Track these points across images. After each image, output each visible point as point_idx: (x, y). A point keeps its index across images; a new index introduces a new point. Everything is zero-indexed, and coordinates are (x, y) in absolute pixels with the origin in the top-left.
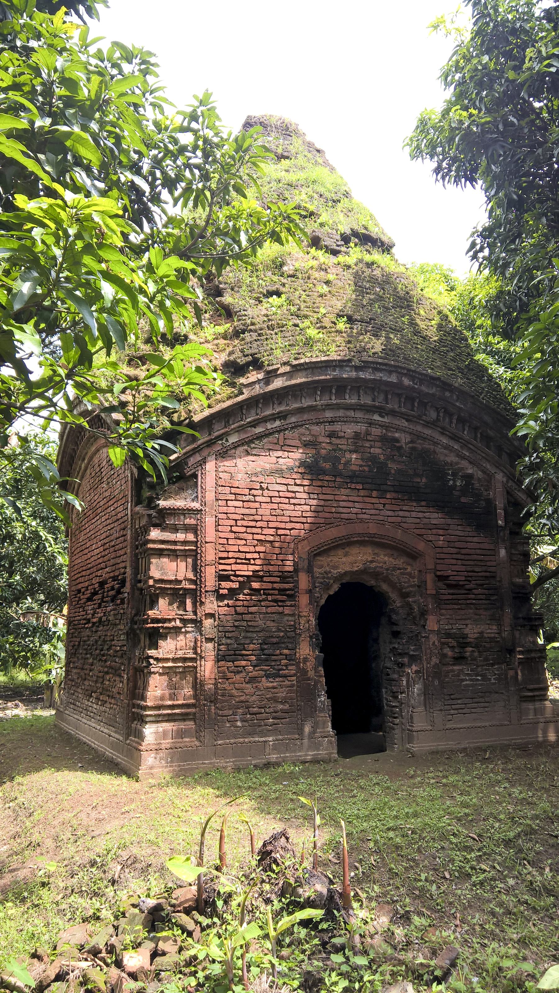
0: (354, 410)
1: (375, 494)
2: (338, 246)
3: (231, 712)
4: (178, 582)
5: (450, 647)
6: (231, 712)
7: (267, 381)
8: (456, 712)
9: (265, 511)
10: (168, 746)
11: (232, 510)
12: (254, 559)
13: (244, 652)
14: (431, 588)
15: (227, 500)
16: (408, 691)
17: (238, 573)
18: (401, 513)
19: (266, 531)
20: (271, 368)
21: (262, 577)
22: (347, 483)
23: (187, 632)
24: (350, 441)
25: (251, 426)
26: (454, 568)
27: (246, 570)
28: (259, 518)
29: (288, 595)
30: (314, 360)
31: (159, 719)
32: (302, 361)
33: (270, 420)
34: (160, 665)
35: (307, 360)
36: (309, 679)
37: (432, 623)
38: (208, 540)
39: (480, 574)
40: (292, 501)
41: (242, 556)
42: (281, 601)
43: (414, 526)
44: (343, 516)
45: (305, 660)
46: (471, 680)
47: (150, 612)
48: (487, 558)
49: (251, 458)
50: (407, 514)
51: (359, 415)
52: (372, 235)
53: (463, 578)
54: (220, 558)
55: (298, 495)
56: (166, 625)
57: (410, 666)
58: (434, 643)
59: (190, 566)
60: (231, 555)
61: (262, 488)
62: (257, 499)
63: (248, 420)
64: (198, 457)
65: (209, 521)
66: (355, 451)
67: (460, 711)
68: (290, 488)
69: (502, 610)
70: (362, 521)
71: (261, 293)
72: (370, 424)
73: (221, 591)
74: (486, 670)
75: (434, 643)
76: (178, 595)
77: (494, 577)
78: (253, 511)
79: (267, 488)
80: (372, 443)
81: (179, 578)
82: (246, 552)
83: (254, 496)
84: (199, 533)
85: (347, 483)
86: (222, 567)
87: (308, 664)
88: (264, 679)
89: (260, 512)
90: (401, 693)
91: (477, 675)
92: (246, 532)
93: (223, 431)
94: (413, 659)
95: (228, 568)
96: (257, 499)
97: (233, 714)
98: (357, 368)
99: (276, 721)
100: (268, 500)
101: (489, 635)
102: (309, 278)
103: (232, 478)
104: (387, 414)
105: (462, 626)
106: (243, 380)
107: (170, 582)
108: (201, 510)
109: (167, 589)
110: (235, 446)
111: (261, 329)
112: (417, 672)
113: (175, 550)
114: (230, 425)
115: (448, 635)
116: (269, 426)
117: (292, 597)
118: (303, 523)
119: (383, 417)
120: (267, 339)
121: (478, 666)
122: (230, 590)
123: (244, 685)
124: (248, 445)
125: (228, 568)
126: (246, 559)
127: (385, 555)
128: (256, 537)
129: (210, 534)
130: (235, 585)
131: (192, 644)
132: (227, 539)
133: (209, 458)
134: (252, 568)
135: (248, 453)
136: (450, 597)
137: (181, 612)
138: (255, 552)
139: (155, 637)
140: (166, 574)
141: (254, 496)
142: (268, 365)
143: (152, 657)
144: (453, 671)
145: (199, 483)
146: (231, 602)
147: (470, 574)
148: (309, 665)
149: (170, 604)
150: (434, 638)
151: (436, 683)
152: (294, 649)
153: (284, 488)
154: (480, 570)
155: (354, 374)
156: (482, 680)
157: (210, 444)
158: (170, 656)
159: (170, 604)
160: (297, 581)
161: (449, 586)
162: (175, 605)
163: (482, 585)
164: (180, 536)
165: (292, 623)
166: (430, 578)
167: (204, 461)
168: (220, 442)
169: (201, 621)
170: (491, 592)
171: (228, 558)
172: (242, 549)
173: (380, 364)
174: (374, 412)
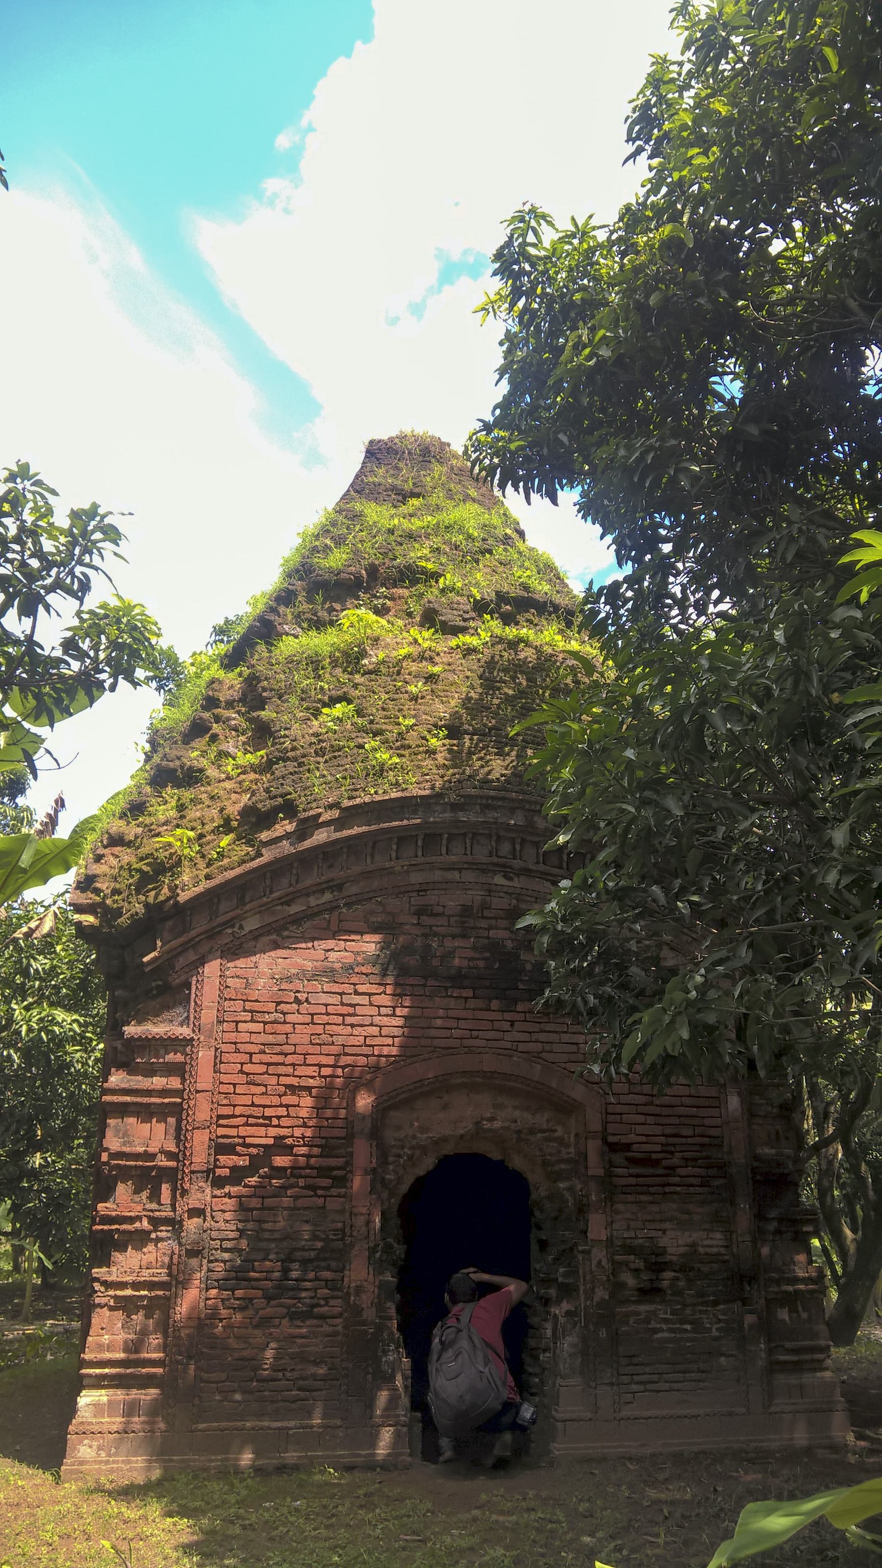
0: (460, 870)
1: (495, 1004)
2: (465, 620)
3: (224, 1376)
4: (152, 1157)
5: (631, 1270)
6: (224, 1376)
7: (302, 833)
8: (642, 1388)
9: (302, 1037)
10: (115, 1428)
11: (245, 1037)
12: (279, 1118)
13: (252, 1274)
14: (595, 1168)
15: (237, 1022)
16: (555, 1348)
17: (248, 1140)
18: (542, 1037)
19: (300, 1071)
20: (307, 814)
21: (291, 1147)
22: (446, 988)
23: (159, 1240)
24: (452, 919)
25: (282, 904)
26: (640, 1129)
27: (263, 1137)
28: (289, 1049)
29: (334, 1178)
30: (378, 798)
31: (98, 1383)
32: (358, 801)
33: (314, 892)
34: (111, 1293)
35: (367, 799)
36: (364, 1323)
37: (597, 1226)
38: (199, 1087)
39: (689, 1140)
40: (349, 1020)
41: (258, 1112)
42: (323, 1188)
43: (565, 1057)
44: (436, 1042)
45: (359, 1290)
46: (671, 1330)
47: (100, 1206)
48: (703, 1112)
49: (281, 953)
50: (554, 1037)
51: (469, 876)
52: (536, 597)
53: (658, 1148)
54: (220, 1117)
55: (359, 1010)
56: (125, 1227)
57: (558, 1302)
58: (600, 1262)
59: (172, 1131)
60: (238, 1111)
61: (297, 1001)
62: (289, 1018)
63: (275, 895)
64: (192, 956)
65: (205, 1055)
66: (464, 936)
67: (649, 1386)
68: (346, 999)
69: (733, 1203)
70: (470, 1050)
71: (320, 700)
72: (490, 891)
73: (219, 1172)
74: (701, 1312)
75: (600, 1262)
76: (147, 1177)
77: (721, 1146)
78: (282, 1039)
79: (307, 1000)
80: (493, 922)
81: (151, 1150)
82: (264, 1106)
83: (284, 1014)
84: (187, 1077)
85: (446, 988)
86: (221, 1131)
87: (364, 1297)
88: (285, 1322)
89: (293, 1039)
90: (545, 1351)
91: (683, 1322)
92: (266, 1073)
93: (231, 915)
94: (567, 1291)
95: (233, 1132)
96: (289, 1018)
97: (228, 1379)
98: (455, 807)
99: (302, 1394)
100: (308, 1019)
101: (709, 1250)
102: (399, 673)
103: (248, 985)
104: (518, 875)
105: (653, 1234)
106: (264, 836)
107: (137, 1156)
108: (192, 1039)
109: (130, 1167)
110: (256, 935)
111: (304, 756)
112: (568, 1313)
113: (149, 1105)
114: (244, 904)
115: (629, 1250)
116: (313, 901)
117: (342, 1181)
118: (367, 1056)
119: (511, 879)
120: (309, 770)
121: (685, 1306)
122: (234, 1169)
123: (250, 1330)
124: (279, 934)
125: (233, 1132)
126: (264, 1117)
127: (515, 1108)
128: (284, 1080)
129: (204, 1077)
130: (243, 1162)
131: (167, 1260)
132: (234, 1085)
133: (210, 957)
134: (273, 1132)
135: (276, 946)
136: (633, 1181)
137: (154, 1206)
138: (281, 1105)
139: (105, 1247)
140: (131, 1144)
141: (284, 1014)
142: (304, 810)
143: (97, 1280)
144: (637, 1313)
145: (193, 996)
146: (234, 1190)
147: (671, 1140)
148: (365, 1300)
149: (137, 1192)
150: (599, 1254)
151: (603, 1334)
152: (342, 1270)
153: (336, 999)
154: (690, 1132)
155: (448, 815)
156: (694, 1331)
157: (212, 935)
158: (128, 1279)
159: (137, 1192)
160: (351, 1154)
161: (633, 1161)
162: (145, 1194)
163: (695, 1160)
164: (158, 1082)
165: (340, 1225)
166: (593, 1147)
167: (202, 961)
168: (229, 931)
169: (182, 1220)
170: (713, 1172)
171: (234, 1116)
172: (257, 1101)
173: (493, 798)
174: (495, 873)
